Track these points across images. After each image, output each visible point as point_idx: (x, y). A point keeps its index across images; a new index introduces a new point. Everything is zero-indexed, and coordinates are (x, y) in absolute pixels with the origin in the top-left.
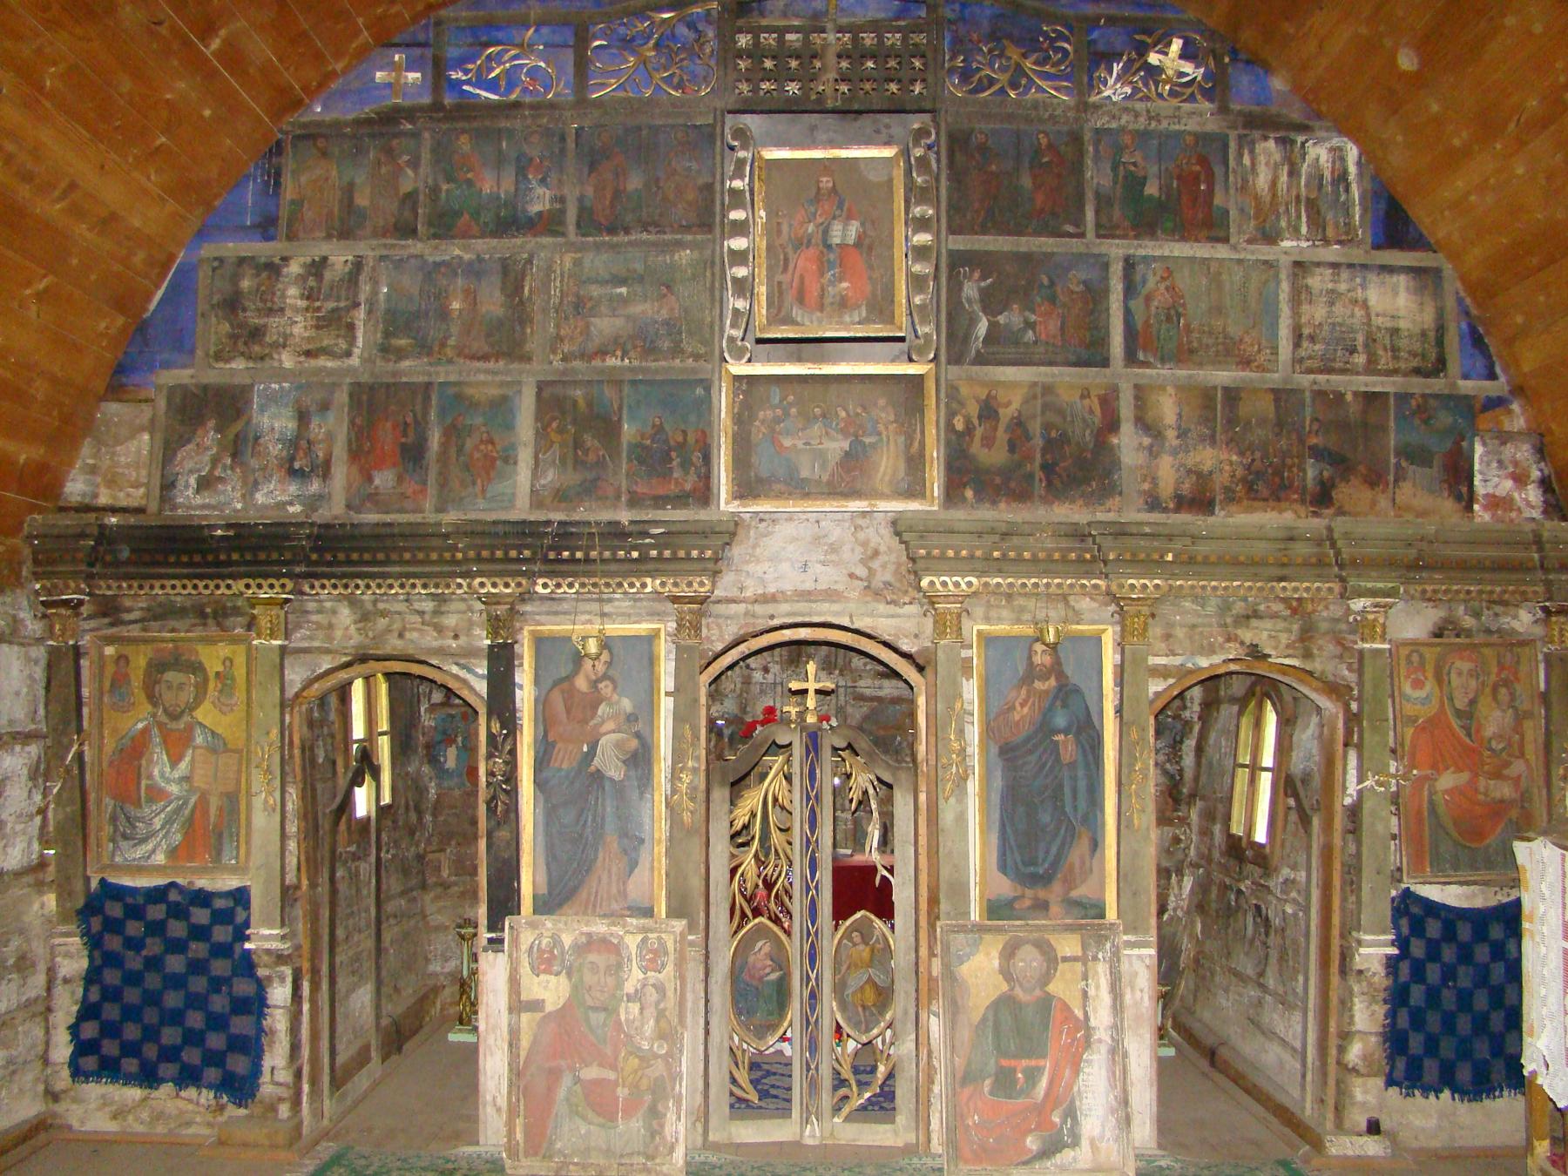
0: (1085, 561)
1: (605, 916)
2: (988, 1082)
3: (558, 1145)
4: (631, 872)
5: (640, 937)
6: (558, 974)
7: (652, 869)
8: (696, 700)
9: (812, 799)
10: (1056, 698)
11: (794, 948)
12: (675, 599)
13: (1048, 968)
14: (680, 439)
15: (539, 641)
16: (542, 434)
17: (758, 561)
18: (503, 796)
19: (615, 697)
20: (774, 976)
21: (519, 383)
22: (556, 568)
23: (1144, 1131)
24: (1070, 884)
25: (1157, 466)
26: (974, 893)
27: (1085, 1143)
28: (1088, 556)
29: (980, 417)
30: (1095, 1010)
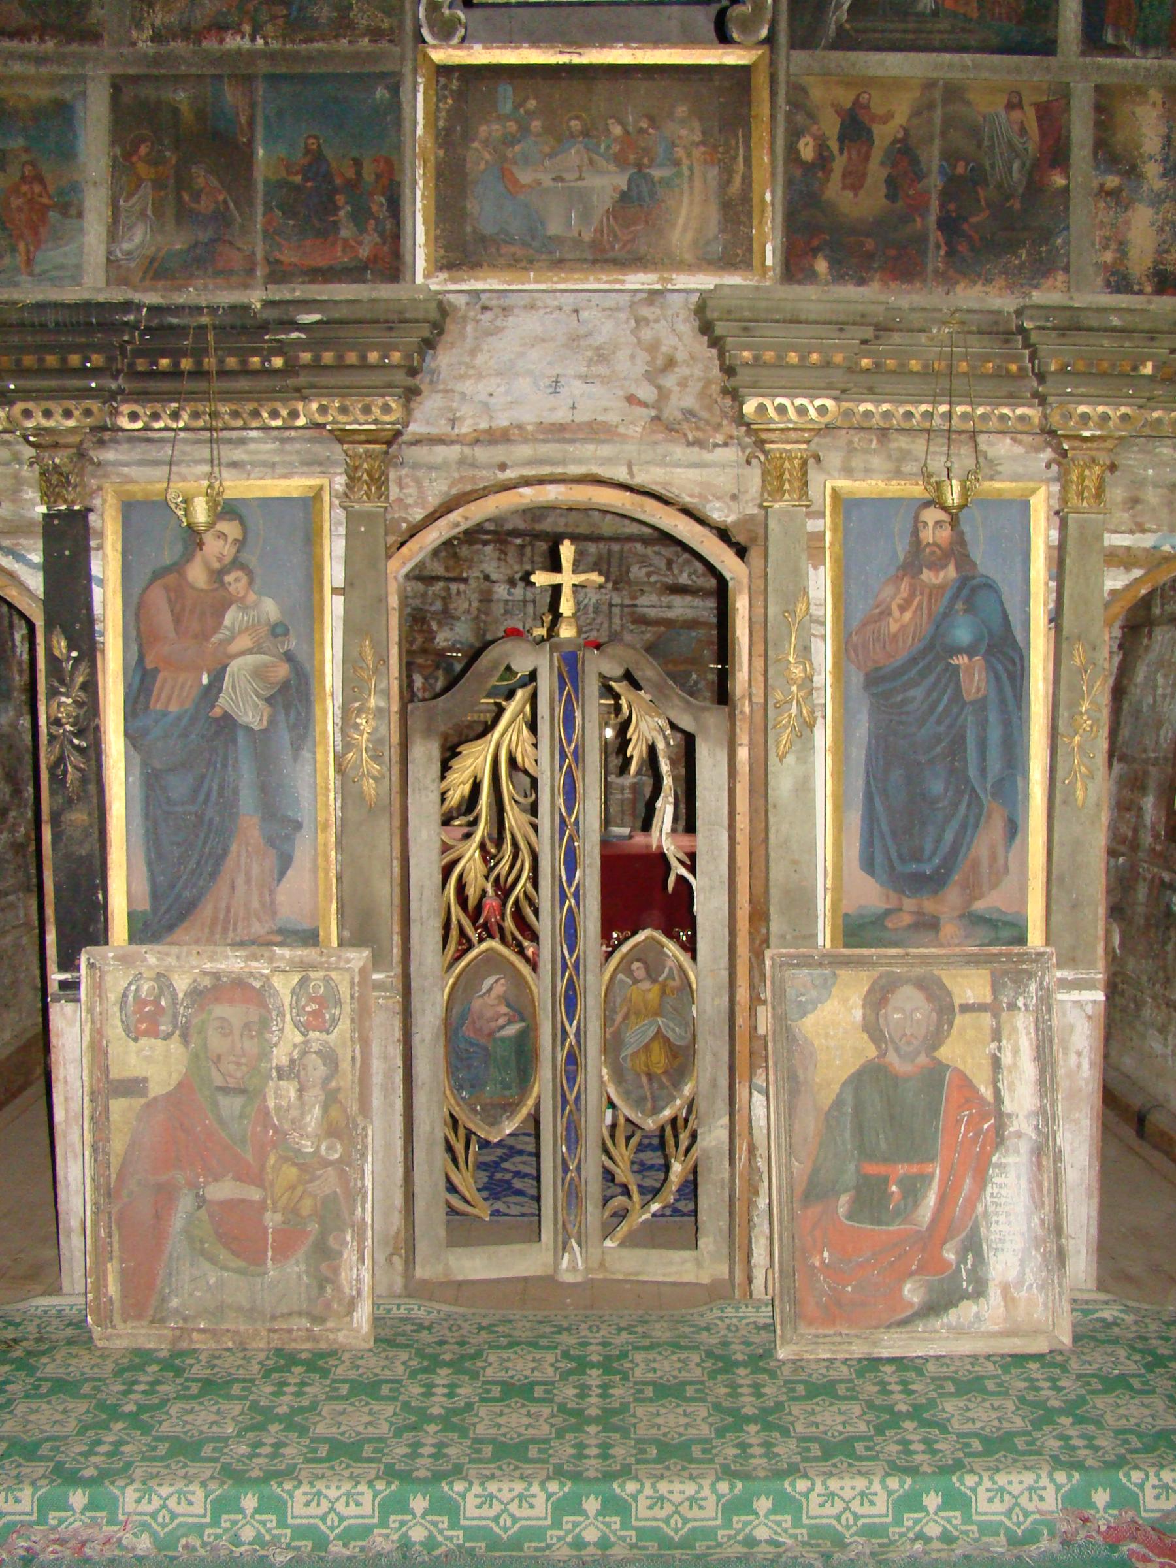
0: (1009, 375)
1: (241, 944)
2: (844, 1199)
3: (175, 1303)
4: (282, 873)
5: (295, 978)
6: (168, 1037)
7: (315, 870)
8: (383, 599)
9: (570, 758)
10: (955, 597)
11: (543, 987)
12: (342, 436)
13: (939, 1027)
14: (351, 174)
15: (129, 509)
16: (122, 167)
17: (480, 376)
18: (75, 758)
19: (252, 597)
20: (512, 1030)
21: (82, 79)
22: (152, 386)
23: (1081, 1264)
24: (973, 890)
25: (1127, 222)
26: (823, 905)
27: (994, 1293)
28: (1013, 368)
29: (842, 139)
30: (1012, 1089)
